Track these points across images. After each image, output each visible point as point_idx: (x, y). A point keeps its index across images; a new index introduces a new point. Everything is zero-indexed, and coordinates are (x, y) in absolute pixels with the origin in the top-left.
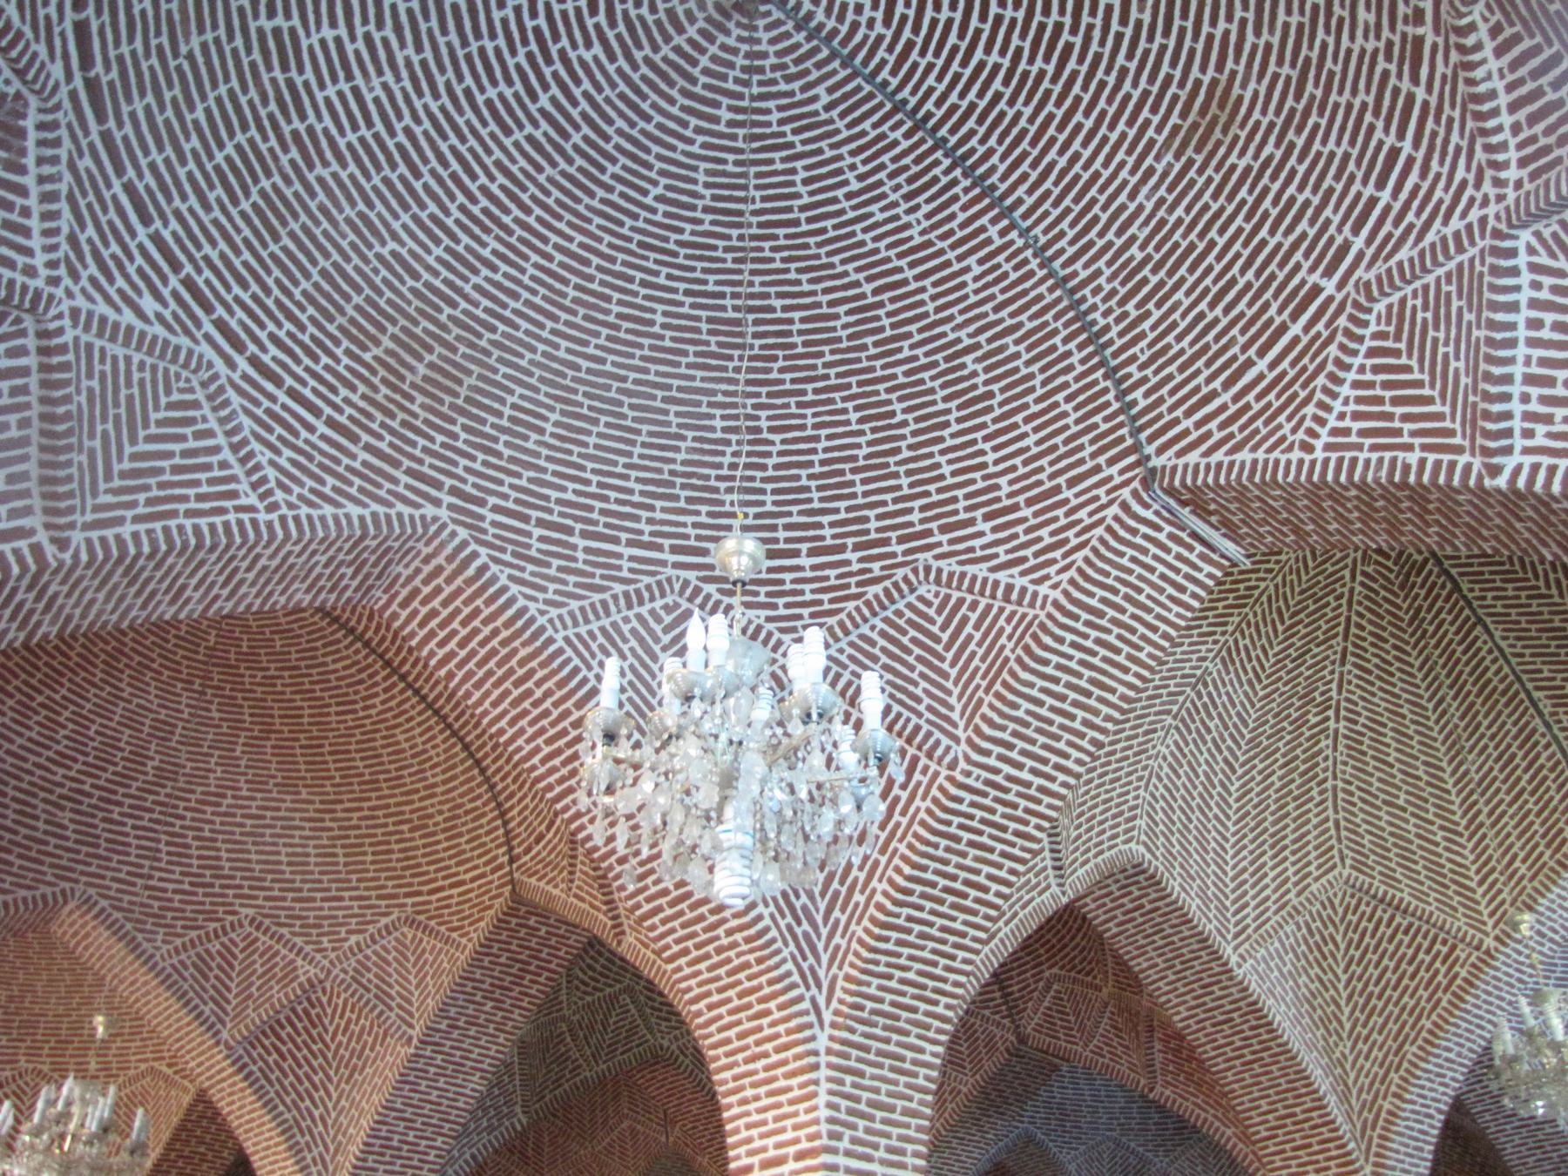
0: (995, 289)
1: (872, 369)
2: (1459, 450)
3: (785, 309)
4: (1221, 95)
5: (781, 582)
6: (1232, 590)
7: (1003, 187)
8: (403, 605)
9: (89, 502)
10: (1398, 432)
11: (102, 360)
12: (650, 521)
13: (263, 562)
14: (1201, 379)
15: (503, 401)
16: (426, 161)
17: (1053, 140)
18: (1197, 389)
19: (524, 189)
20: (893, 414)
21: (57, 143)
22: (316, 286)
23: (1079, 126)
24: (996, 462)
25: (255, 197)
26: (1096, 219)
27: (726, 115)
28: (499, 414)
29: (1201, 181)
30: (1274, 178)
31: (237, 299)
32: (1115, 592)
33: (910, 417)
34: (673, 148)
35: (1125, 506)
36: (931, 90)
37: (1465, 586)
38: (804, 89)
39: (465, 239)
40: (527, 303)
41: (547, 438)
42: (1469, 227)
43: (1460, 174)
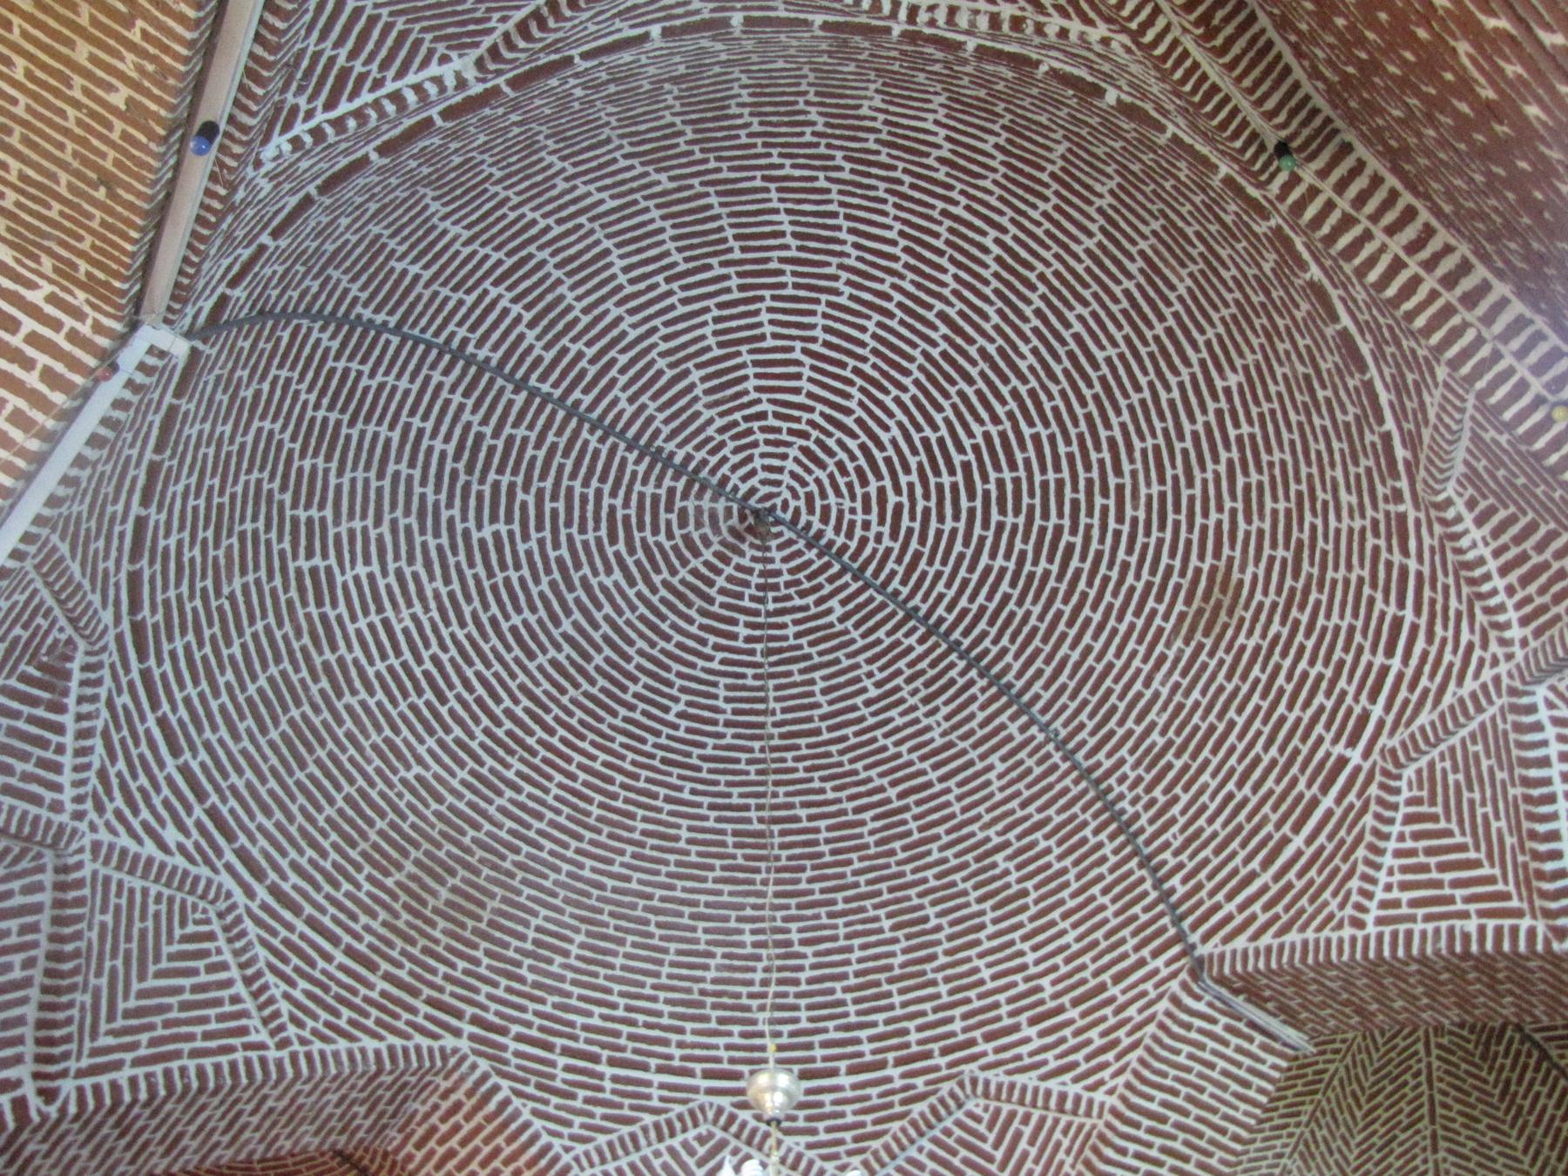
0: (1020, 786)
1: (902, 874)
2: (1519, 914)
3: (811, 818)
4: (1221, 580)
5: (820, 1105)
6: (1301, 1080)
7: (1019, 684)
8: (419, 1146)
9: (87, 1045)
10: (1450, 900)
11: (119, 895)
12: (681, 1045)
13: (270, 1103)
14: (1238, 860)
15: (526, 924)
16: (451, 686)
17: (1064, 636)
18: (1235, 872)
19: (548, 710)
20: (925, 919)
21: (98, 682)
22: (341, 812)
23: (1088, 621)
24: (1037, 962)
25: (284, 726)
26: (1114, 709)
27: (743, 632)
28: (523, 938)
29: (1213, 663)
30: (1284, 654)
31: (260, 828)
32: (1175, 1093)
33: (944, 921)
34: (693, 666)
35: (1175, 1000)
36: (941, 596)
37: (1554, 1053)
38: (818, 603)
39: (490, 762)
40: (552, 823)
41: (573, 961)
42: (1484, 687)
43: (1465, 637)
